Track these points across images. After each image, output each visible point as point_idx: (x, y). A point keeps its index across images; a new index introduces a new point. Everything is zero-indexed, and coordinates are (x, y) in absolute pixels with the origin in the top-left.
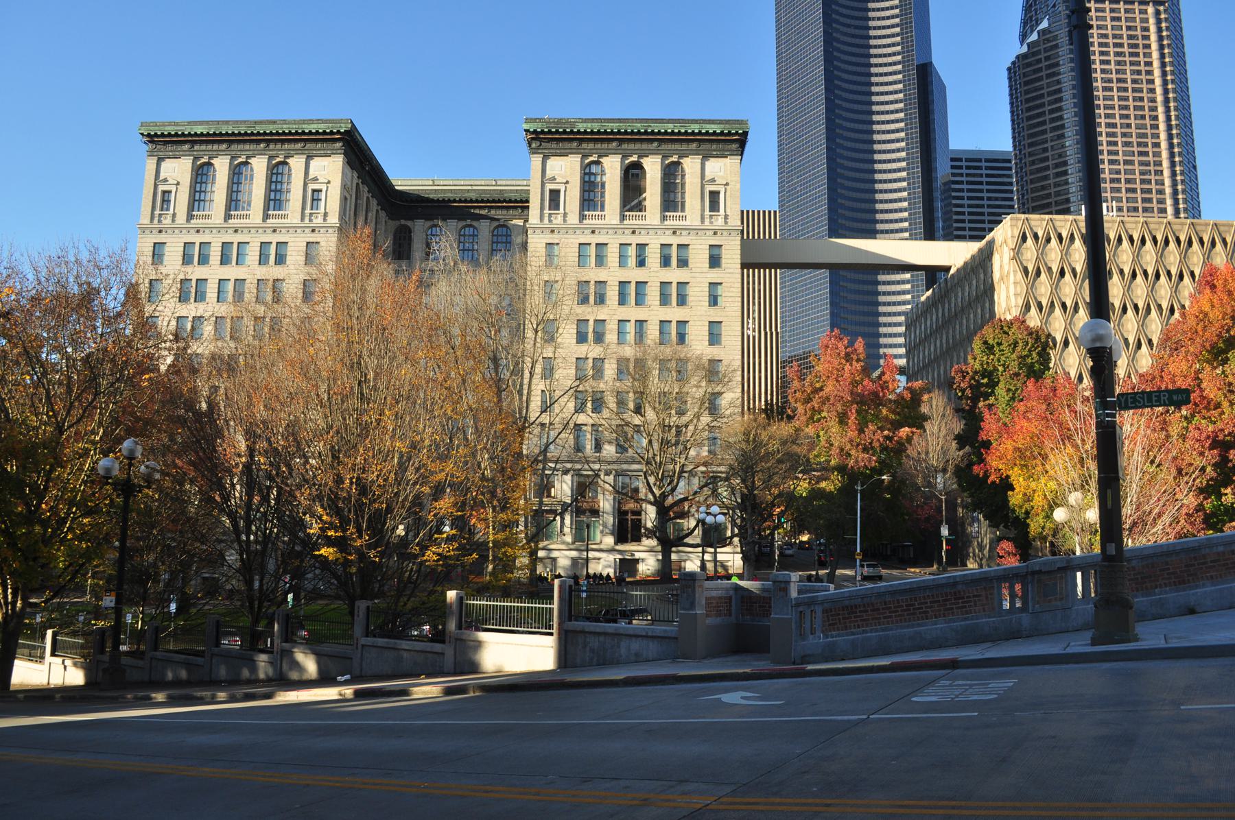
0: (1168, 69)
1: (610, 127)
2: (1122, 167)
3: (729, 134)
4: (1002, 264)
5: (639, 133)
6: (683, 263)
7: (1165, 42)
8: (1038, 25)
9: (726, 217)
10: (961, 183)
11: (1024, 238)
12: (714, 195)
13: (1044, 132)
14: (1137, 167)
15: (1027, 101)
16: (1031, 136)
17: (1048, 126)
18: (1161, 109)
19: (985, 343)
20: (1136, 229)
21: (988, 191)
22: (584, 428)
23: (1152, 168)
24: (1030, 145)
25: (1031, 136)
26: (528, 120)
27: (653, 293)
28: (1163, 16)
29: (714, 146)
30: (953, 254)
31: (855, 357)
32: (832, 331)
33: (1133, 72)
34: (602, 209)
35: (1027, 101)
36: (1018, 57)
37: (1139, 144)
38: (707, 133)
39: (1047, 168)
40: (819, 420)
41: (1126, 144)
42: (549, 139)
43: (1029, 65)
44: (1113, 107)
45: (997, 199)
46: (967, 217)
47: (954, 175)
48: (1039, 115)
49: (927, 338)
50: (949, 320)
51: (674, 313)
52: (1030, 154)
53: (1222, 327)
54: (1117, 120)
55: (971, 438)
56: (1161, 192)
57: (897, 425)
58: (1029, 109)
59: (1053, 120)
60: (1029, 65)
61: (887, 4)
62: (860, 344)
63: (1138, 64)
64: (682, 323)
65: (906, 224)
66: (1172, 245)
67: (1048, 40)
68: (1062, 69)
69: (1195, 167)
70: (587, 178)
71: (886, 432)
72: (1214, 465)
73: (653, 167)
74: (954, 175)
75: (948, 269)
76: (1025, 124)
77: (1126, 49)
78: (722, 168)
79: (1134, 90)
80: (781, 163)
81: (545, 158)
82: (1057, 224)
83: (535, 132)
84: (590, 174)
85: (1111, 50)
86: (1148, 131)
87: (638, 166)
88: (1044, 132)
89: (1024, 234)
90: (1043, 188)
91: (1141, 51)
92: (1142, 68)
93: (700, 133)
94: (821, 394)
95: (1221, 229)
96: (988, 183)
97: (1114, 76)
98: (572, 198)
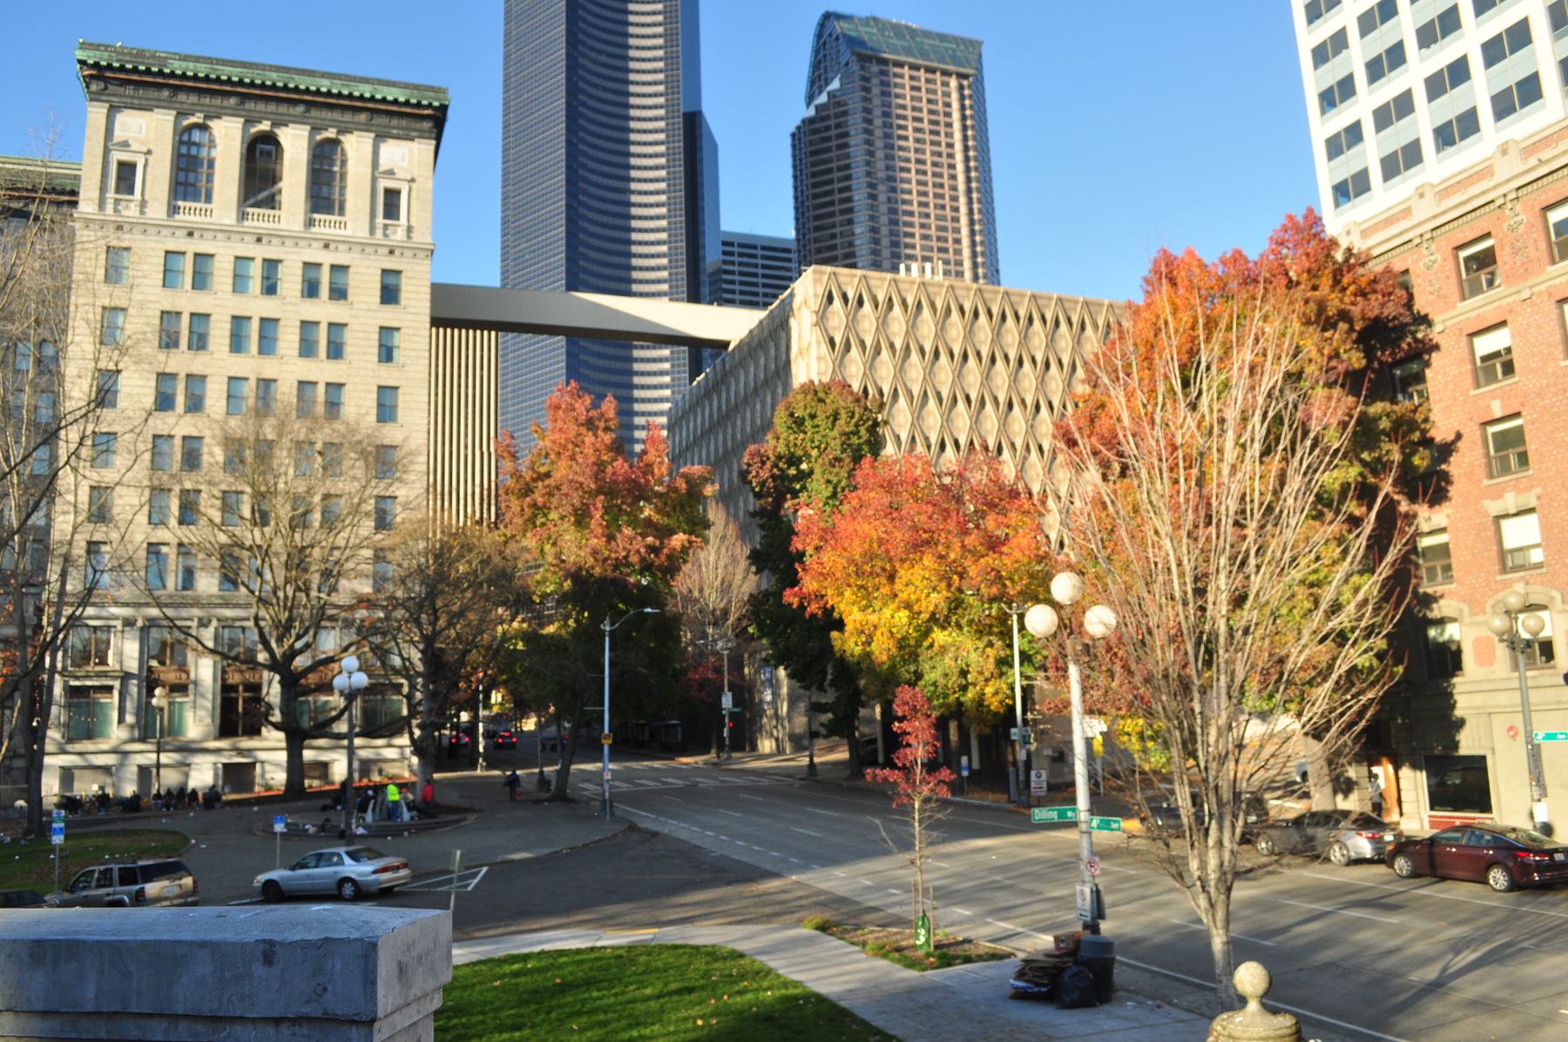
1: (225, 72)
4: (802, 329)
5: (274, 87)
6: (339, 293)
9: (409, 229)
10: (733, 273)
11: (830, 299)
12: (392, 196)
13: (832, 214)
15: (814, 175)
16: (817, 218)
18: (962, 200)
21: (765, 285)
22: (164, 549)
24: (817, 229)
25: (817, 218)
26: (84, 46)
27: (289, 338)
29: (394, 122)
30: (729, 324)
31: (602, 424)
32: (568, 383)
34: (208, 199)
35: (814, 175)
36: (804, 121)
37: (939, 239)
38: (384, 100)
42: (120, 80)
43: (816, 131)
47: (725, 262)
50: (727, 414)
51: (322, 370)
52: (816, 240)
55: (776, 553)
58: (815, 185)
60: (816, 131)
61: (649, 8)
62: (609, 406)
64: (335, 387)
68: (852, 141)
70: (184, 150)
71: (650, 539)
73: (295, 142)
74: (725, 262)
75: (726, 344)
76: (811, 203)
77: (925, 125)
78: (406, 156)
79: (934, 175)
80: (505, 198)
81: (113, 110)
82: (872, 283)
83: (96, 65)
84: (190, 143)
87: (270, 139)
91: (942, 129)
93: (372, 99)
94: (547, 482)
95: (1067, 305)
96: (764, 276)
98: (156, 177)
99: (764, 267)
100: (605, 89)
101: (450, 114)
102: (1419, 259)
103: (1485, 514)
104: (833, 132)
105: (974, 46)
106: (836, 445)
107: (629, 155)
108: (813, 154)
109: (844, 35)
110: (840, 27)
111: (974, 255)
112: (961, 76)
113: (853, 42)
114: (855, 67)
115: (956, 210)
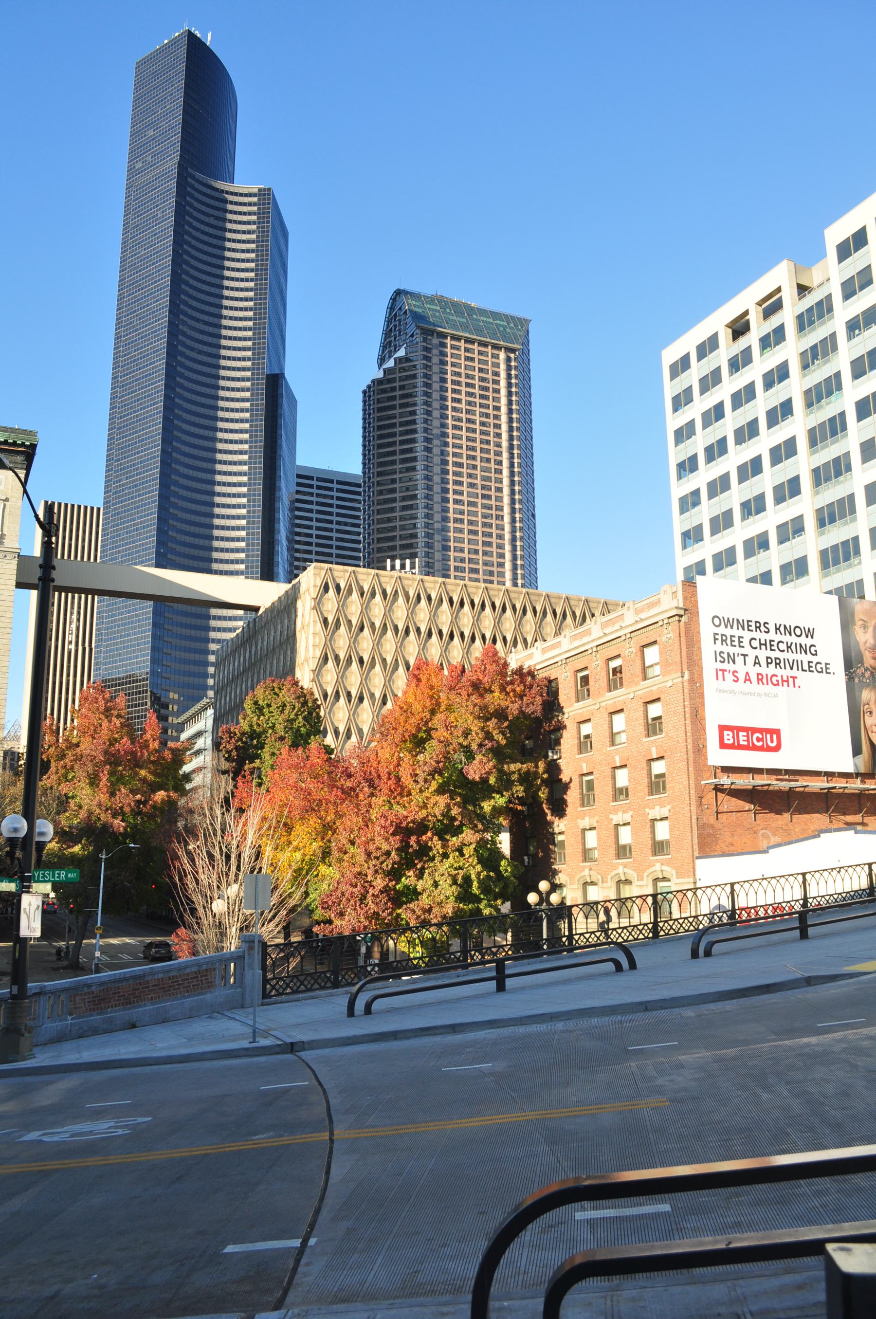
0: (514, 416)
2: (465, 508)
3: (14, 444)
4: (304, 607)
7: (514, 390)
8: (396, 351)
13: (393, 462)
14: (479, 509)
15: (380, 428)
16: (380, 464)
17: (398, 457)
18: (505, 455)
19: (256, 703)
20: (434, 588)
21: (338, 515)
23: (493, 512)
24: (380, 474)
28: (513, 364)
30: (265, 594)
33: (482, 415)
35: (380, 428)
36: (373, 381)
39: (394, 500)
40: (72, 779)
41: (472, 485)
43: (383, 391)
44: (461, 447)
45: (346, 524)
46: (314, 540)
48: (389, 445)
49: (235, 679)
50: (255, 664)
52: (379, 484)
53: (422, 719)
54: (464, 460)
56: (500, 537)
57: (154, 788)
58: (380, 437)
59: (403, 452)
60: (383, 391)
63: (488, 407)
65: (243, 544)
66: (467, 607)
67: (404, 369)
69: (533, 516)
71: (138, 797)
72: (397, 850)
77: (477, 391)
85: (463, 389)
86: (492, 475)
88: (393, 462)
89: (327, 584)
90: (389, 520)
92: (491, 411)
96: (338, 507)
97: (464, 416)
99: (338, 498)
100: (200, 352)
101: (38, 450)
102: (562, 673)
103: (578, 827)
104: (397, 393)
105: (522, 324)
106: (280, 728)
107: (217, 408)
108: (380, 410)
109: (411, 311)
110: (408, 304)
111: (513, 501)
112: (509, 350)
113: (418, 317)
114: (419, 339)
115: (500, 463)
